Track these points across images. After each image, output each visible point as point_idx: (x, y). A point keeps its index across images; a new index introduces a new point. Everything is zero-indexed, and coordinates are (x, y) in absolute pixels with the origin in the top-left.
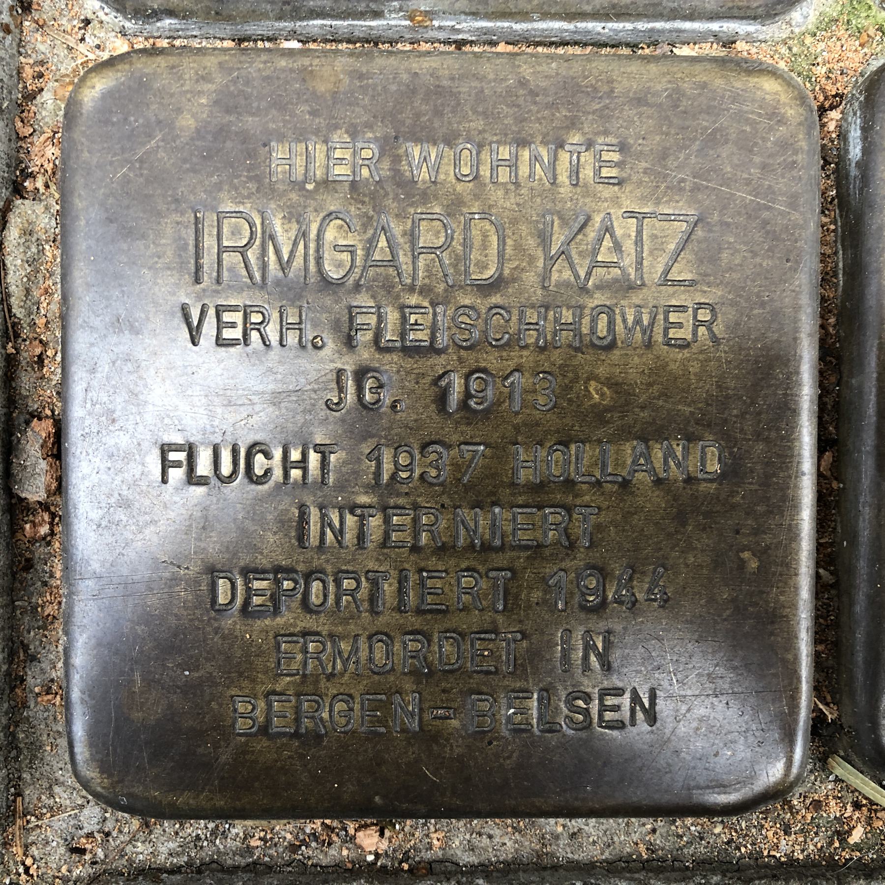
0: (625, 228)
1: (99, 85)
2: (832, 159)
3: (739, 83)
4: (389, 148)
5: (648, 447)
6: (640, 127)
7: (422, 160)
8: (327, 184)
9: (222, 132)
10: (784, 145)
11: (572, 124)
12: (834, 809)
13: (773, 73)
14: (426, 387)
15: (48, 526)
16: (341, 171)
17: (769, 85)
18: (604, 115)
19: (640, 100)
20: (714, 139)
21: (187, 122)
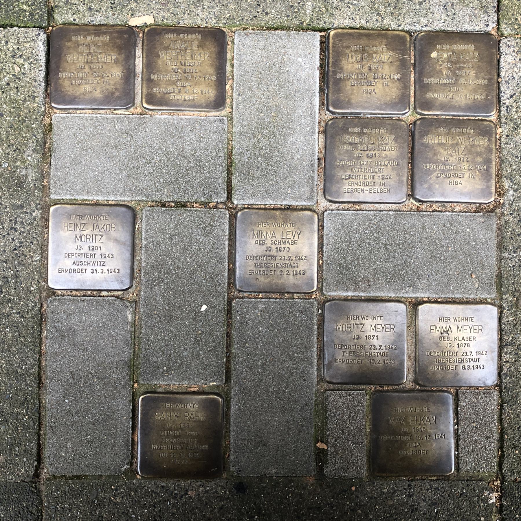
0: (387, 138)
1: (331, 122)
2: (410, 130)
3: (400, 122)
4: (362, 129)
5: (119, 98)
6: (389, 127)
7: (365, 130)
8: (355, 133)
9: (344, 127)
10: (405, 129)
11: (382, 127)
12: (411, 206)
13: (404, 121)
14: (161, 92)
15: (498, 131)
16: (357, 132)
17: (403, 123)
18: (385, 126)
19: (389, 124)
20: (397, 128)
21: (340, 126)
